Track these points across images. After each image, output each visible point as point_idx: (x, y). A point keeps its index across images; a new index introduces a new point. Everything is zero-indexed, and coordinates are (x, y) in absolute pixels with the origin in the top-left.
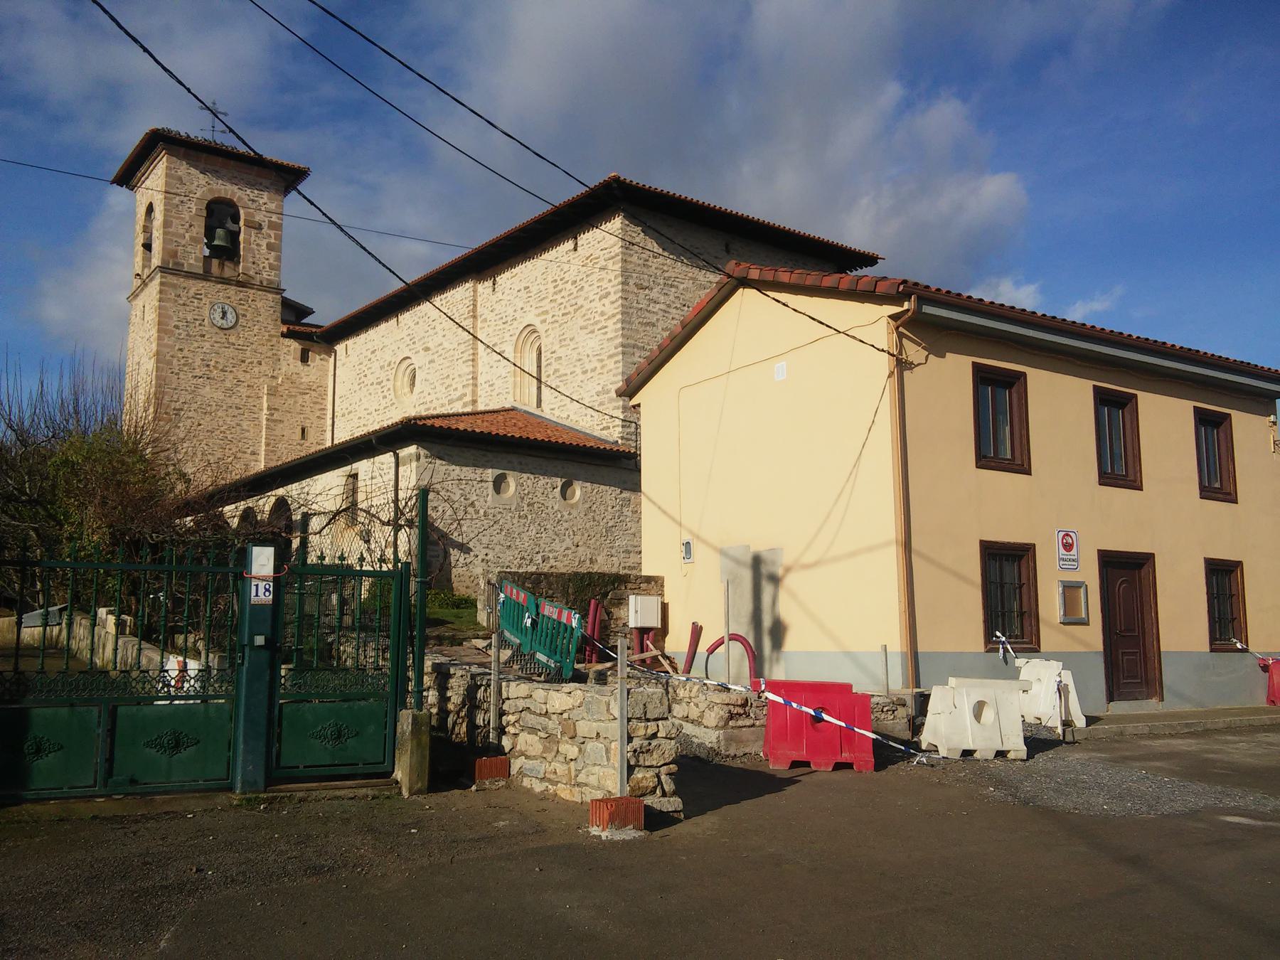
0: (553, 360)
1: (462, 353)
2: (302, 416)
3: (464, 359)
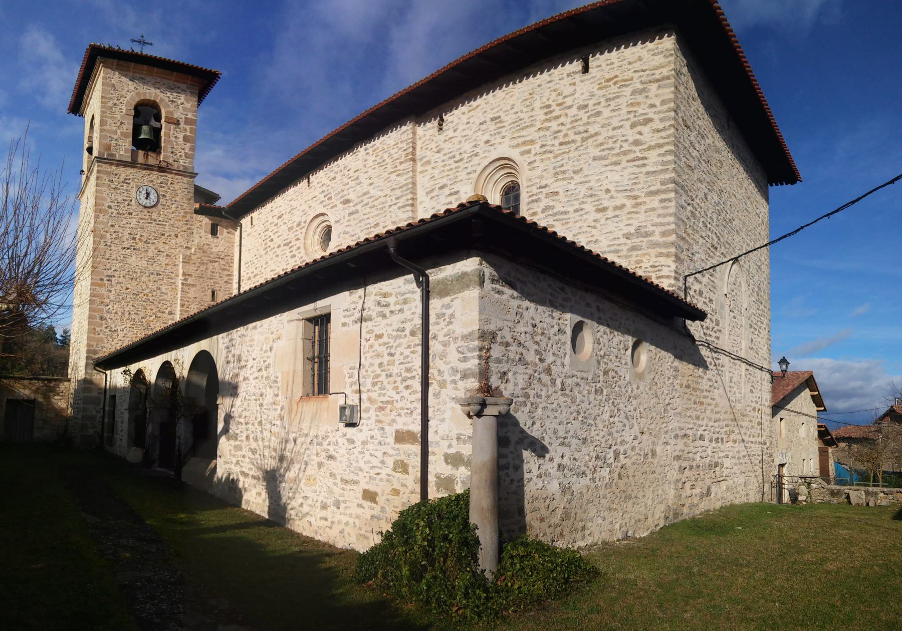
0: (542, 196)
1: (397, 198)
2: (212, 281)
3: (399, 205)
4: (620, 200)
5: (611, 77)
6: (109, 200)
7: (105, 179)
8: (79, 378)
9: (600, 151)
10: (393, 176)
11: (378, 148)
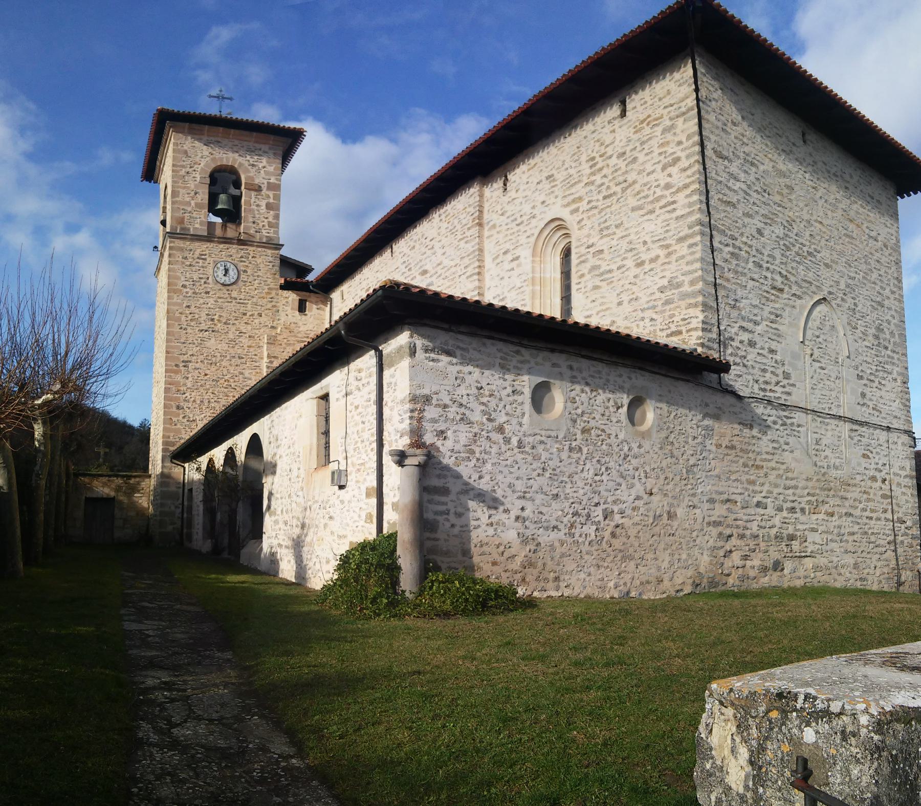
0: (590, 256)
3: (468, 274)
4: (657, 251)
5: (645, 117)
6: (183, 279)
7: (179, 256)
8: (158, 473)
9: (638, 200)
10: (462, 243)
11: (449, 214)
